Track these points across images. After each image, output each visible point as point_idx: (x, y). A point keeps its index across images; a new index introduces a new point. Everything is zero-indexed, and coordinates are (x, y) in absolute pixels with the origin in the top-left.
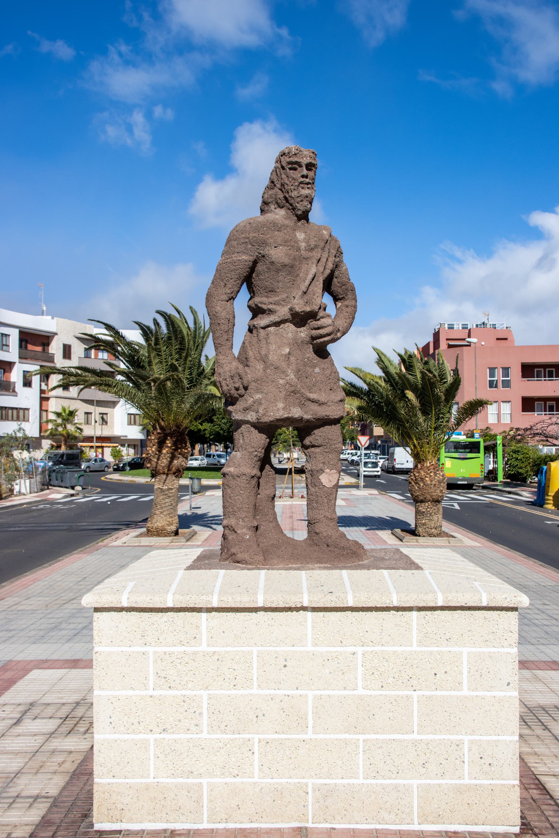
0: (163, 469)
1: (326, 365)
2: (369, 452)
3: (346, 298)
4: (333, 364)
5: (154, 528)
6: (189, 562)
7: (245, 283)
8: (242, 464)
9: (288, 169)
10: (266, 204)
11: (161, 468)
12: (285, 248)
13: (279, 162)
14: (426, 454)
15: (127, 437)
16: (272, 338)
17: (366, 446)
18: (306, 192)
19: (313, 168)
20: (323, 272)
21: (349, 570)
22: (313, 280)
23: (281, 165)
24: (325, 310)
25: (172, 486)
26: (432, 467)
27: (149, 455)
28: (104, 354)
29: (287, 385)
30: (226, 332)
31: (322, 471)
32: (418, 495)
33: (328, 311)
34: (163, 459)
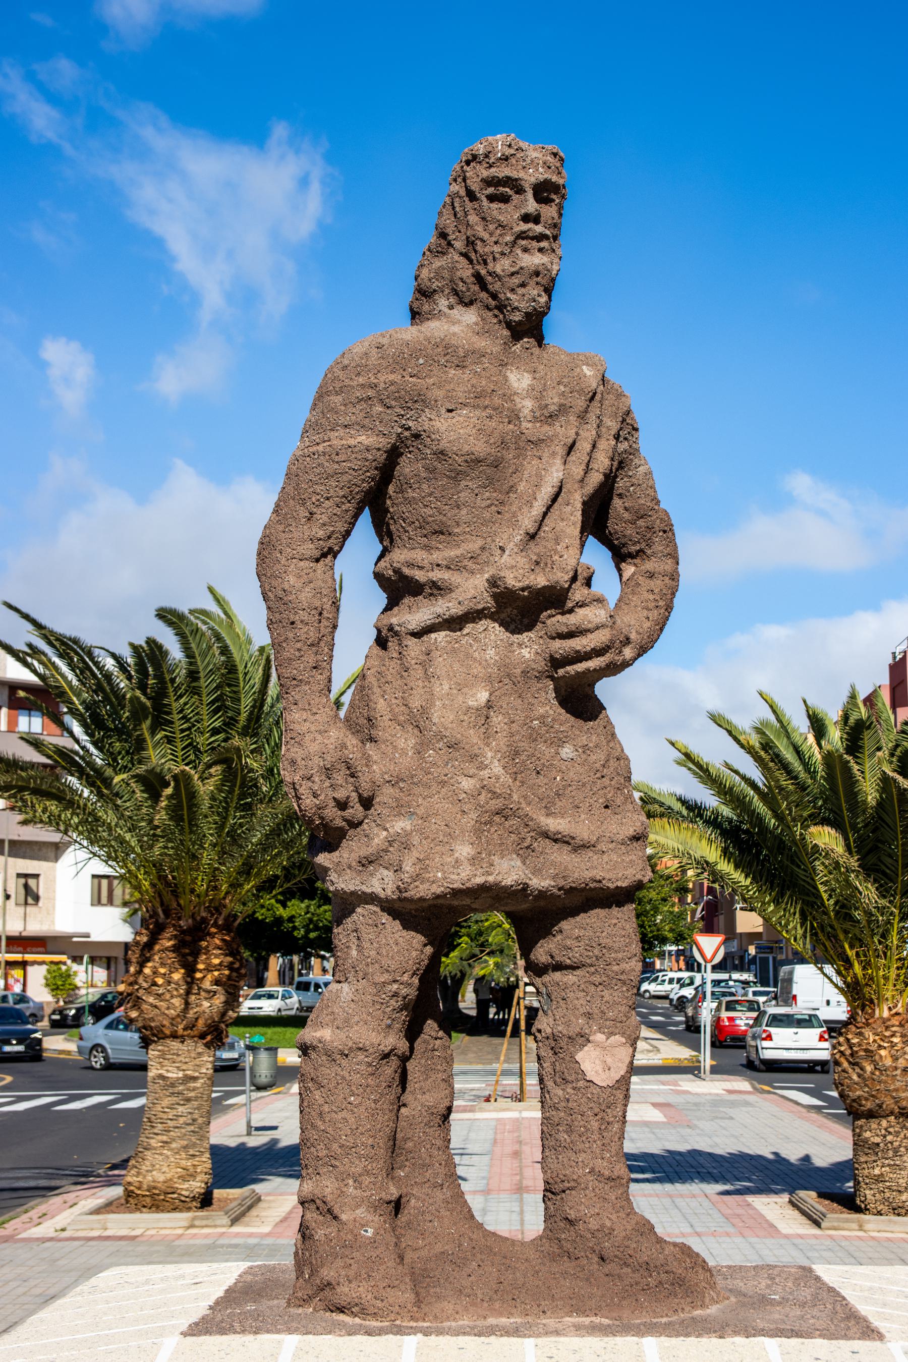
0: (172, 1025)
1: (594, 738)
2: (725, 976)
3: (649, 552)
4: (613, 735)
5: (145, 1187)
6: (200, 1309)
7: (367, 511)
8: (356, 1018)
9: (484, 199)
10: (426, 296)
11: (166, 1023)
12: (478, 412)
13: (459, 180)
14: (878, 986)
15: (88, 937)
16: (440, 663)
17: (717, 960)
18: (534, 260)
19: (554, 197)
20: (582, 481)
21: (663, 1338)
22: (554, 499)
23: (466, 187)
24: (588, 583)
25: (194, 1071)
26: (895, 1021)
27: (137, 987)
28: (33, 719)
29: (484, 794)
30: (312, 645)
31: (583, 1038)
32: (859, 1097)
33: (598, 587)
34: (172, 997)
